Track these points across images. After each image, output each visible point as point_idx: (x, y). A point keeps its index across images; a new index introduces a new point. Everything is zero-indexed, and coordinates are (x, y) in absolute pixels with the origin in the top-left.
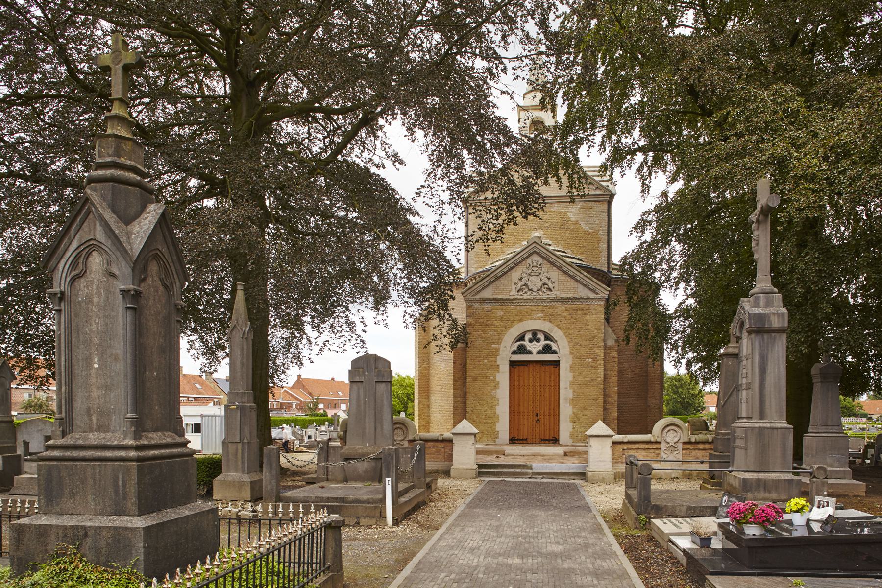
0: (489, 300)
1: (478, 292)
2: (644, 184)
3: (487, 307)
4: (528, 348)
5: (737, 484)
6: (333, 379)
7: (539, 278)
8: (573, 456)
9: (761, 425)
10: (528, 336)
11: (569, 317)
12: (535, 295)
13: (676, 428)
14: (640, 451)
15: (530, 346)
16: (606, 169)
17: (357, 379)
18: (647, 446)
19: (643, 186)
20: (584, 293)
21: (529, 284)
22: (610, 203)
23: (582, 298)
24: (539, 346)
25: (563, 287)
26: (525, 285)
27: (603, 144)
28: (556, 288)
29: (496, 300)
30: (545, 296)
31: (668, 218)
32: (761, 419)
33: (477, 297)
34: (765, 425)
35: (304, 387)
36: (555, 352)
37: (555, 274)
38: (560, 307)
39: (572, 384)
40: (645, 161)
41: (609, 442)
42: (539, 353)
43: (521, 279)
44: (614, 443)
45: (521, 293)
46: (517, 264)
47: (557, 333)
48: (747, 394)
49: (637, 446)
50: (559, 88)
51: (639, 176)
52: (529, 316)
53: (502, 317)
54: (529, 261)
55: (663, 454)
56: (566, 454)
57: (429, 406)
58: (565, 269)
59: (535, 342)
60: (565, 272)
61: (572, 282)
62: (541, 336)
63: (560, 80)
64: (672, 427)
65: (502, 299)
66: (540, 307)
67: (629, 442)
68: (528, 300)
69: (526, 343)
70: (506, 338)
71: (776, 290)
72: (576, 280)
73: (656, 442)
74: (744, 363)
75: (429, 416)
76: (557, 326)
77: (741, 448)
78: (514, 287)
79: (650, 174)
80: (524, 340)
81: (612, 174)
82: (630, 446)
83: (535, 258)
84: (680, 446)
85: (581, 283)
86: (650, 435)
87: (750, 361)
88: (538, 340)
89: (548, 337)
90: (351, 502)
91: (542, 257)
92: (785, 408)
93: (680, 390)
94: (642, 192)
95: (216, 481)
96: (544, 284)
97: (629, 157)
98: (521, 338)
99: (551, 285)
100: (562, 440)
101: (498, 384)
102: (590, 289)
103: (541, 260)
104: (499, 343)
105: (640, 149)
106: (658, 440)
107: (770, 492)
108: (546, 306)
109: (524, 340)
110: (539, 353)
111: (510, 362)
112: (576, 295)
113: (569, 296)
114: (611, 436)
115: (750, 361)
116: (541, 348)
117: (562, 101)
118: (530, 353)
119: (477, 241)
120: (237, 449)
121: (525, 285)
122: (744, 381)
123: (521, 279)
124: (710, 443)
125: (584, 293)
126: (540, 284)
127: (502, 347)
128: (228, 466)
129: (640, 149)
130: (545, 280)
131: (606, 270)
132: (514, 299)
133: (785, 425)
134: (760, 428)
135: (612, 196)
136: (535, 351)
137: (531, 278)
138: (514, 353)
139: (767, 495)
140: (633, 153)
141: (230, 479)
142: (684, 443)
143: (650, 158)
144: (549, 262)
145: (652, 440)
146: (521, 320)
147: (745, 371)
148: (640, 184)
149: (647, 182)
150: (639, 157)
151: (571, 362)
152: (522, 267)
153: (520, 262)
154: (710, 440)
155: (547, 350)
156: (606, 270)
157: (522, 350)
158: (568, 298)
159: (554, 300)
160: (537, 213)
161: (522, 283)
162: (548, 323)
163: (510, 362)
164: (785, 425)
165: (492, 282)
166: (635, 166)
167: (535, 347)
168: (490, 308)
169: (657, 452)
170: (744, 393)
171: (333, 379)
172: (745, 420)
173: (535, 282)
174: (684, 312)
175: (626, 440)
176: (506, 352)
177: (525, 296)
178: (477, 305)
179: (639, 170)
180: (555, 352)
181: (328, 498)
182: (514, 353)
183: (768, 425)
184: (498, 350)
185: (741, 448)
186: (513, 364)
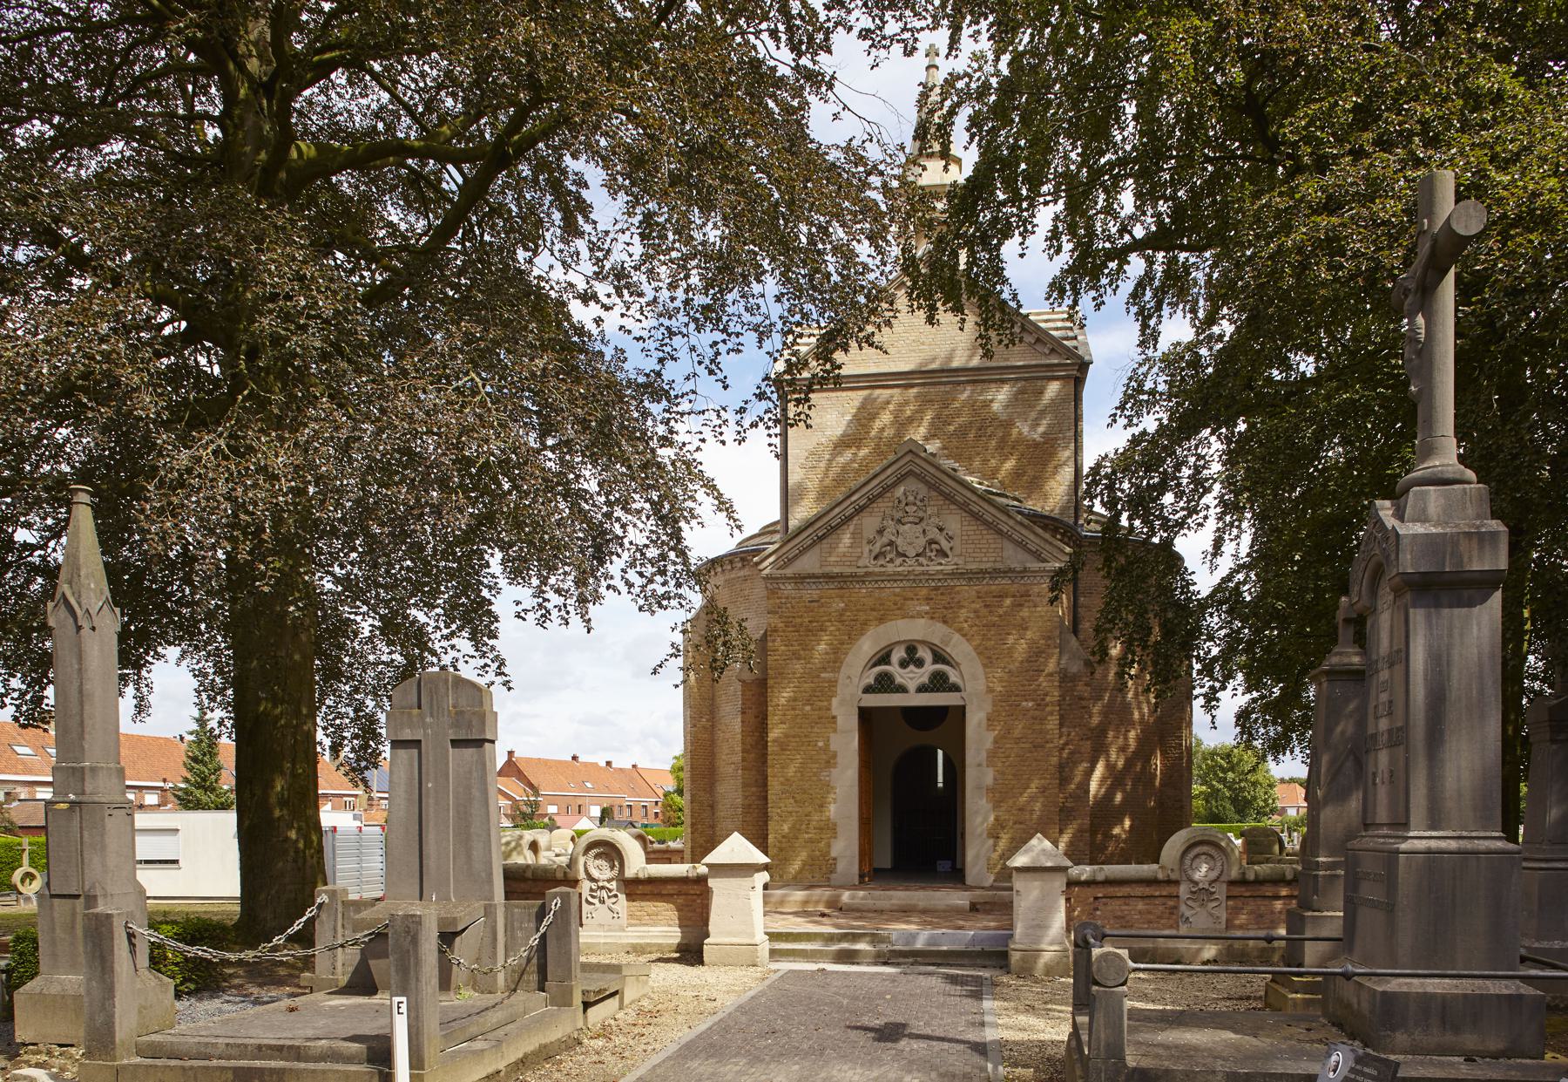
0: (813, 576)
1: (791, 561)
2: (1145, 326)
3: (811, 592)
4: (899, 680)
5: (1365, 1006)
6: (574, 758)
7: (919, 528)
8: (987, 912)
9: (1433, 844)
10: (898, 654)
11: (984, 611)
12: (911, 565)
13: (1213, 852)
14: (1132, 902)
15: (900, 675)
16: (1062, 292)
17: (407, 735)
18: (1148, 891)
19: (1143, 334)
20: (1014, 558)
21: (899, 541)
22: (1079, 382)
23: (1011, 570)
24: (922, 675)
25: (966, 545)
26: (891, 543)
27: (1054, 235)
28: (957, 551)
29: (829, 577)
30: (934, 568)
31: (1201, 395)
32: (1432, 828)
33: (789, 571)
34: (1443, 844)
35: (520, 775)
36: (955, 688)
37: (954, 522)
38: (967, 591)
39: (992, 756)
40: (1148, 276)
41: (1059, 883)
42: (922, 689)
43: (881, 532)
44: (1071, 883)
45: (881, 562)
46: (872, 500)
47: (960, 648)
48: (1393, 761)
49: (1126, 890)
50: (958, 105)
51: (1134, 309)
52: (899, 609)
53: (842, 613)
54: (900, 491)
55: (1183, 908)
56: (974, 908)
57: (712, 807)
58: (975, 508)
59: (912, 667)
60: (976, 516)
61: (990, 537)
62: (925, 654)
63: (960, 84)
64: (1205, 848)
65: (841, 575)
66: (924, 592)
67: (1108, 882)
68: (895, 578)
69: (894, 669)
70: (849, 659)
71: (1470, 474)
72: (1000, 532)
73: (1169, 882)
74: (1384, 675)
75: (713, 827)
76: (960, 630)
77: (1374, 905)
78: (866, 549)
79: (1159, 307)
80: (888, 663)
81: (1076, 303)
82: (1111, 890)
83: (912, 485)
84: (1221, 891)
85: (1010, 538)
86: (1155, 866)
87: (1399, 668)
88: (920, 663)
89: (939, 657)
90: (317, 1059)
91: (926, 483)
92: (117, 1021)
93: (1230, 775)
94: (1142, 344)
95: (20, 996)
96: (932, 542)
97: (1113, 265)
98: (884, 659)
99: (945, 545)
100: (969, 881)
101: (835, 756)
102: (1029, 551)
103: (923, 491)
104: (837, 670)
105: (1137, 246)
106: (1173, 877)
107: (1457, 1030)
108: (936, 588)
109: (888, 663)
110: (922, 689)
111: (860, 709)
112: (998, 565)
113: (983, 566)
114: (1066, 869)
115: (1399, 668)
116: (925, 679)
117: (966, 136)
118: (902, 689)
119: (754, 425)
120: (74, 914)
121: (891, 543)
122: (1383, 724)
123: (881, 532)
124: (1288, 883)
125: (1014, 558)
126: (922, 541)
127: (842, 676)
128: (54, 955)
129: (1137, 246)
130: (933, 533)
131: (1071, 521)
132: (867, 574)
133: (1500, 844)
134: (1429, 852)
135: (1084, 366)
136: (912, 686)
137: (902, 528)
138: (868, 690)
139: (1449, 1038)
140: (1121, 255)
141: (54, 989)
142: (1231, 883)
143: (1159, 269)
144: (941, 493)
145: (1160, 876)
146: (881, 620)
147: (1384, 697)
148: (1137, 326)
149: (1152, 322)
150: (1136, 265)
151: (989, 708)
152: (883, 505)
153: (880, 495)
154: (1289, 876)
155: (939, 683)
156: (1071, 521)
157: (884, 684)
158: (981, 571)
159: (953, 574)
160: (876, 339)
161: (885, 540)
162: (939, 625)
163: (860, 709)
164: (1500, 844)
165: (820, 539)
166: (1126, 287)
167: (910, 678)
168: (815, 594)
169: (1171, 903)
170: (1383, 758)
171: (574, 758)
172: (1385, 831)
173: (910, 538)
174: (1225, 595)
175: (1100, 877)
176: (849, 693)
177: (890, 568)
178: (788, 589)
179: (1136, 296)
180: (955, 688)
181: (260, 1047)
182: (868, 690)
183: (1453, 845)
184: (833, 683)
185: (1374, 905)
186: (865, 715)
